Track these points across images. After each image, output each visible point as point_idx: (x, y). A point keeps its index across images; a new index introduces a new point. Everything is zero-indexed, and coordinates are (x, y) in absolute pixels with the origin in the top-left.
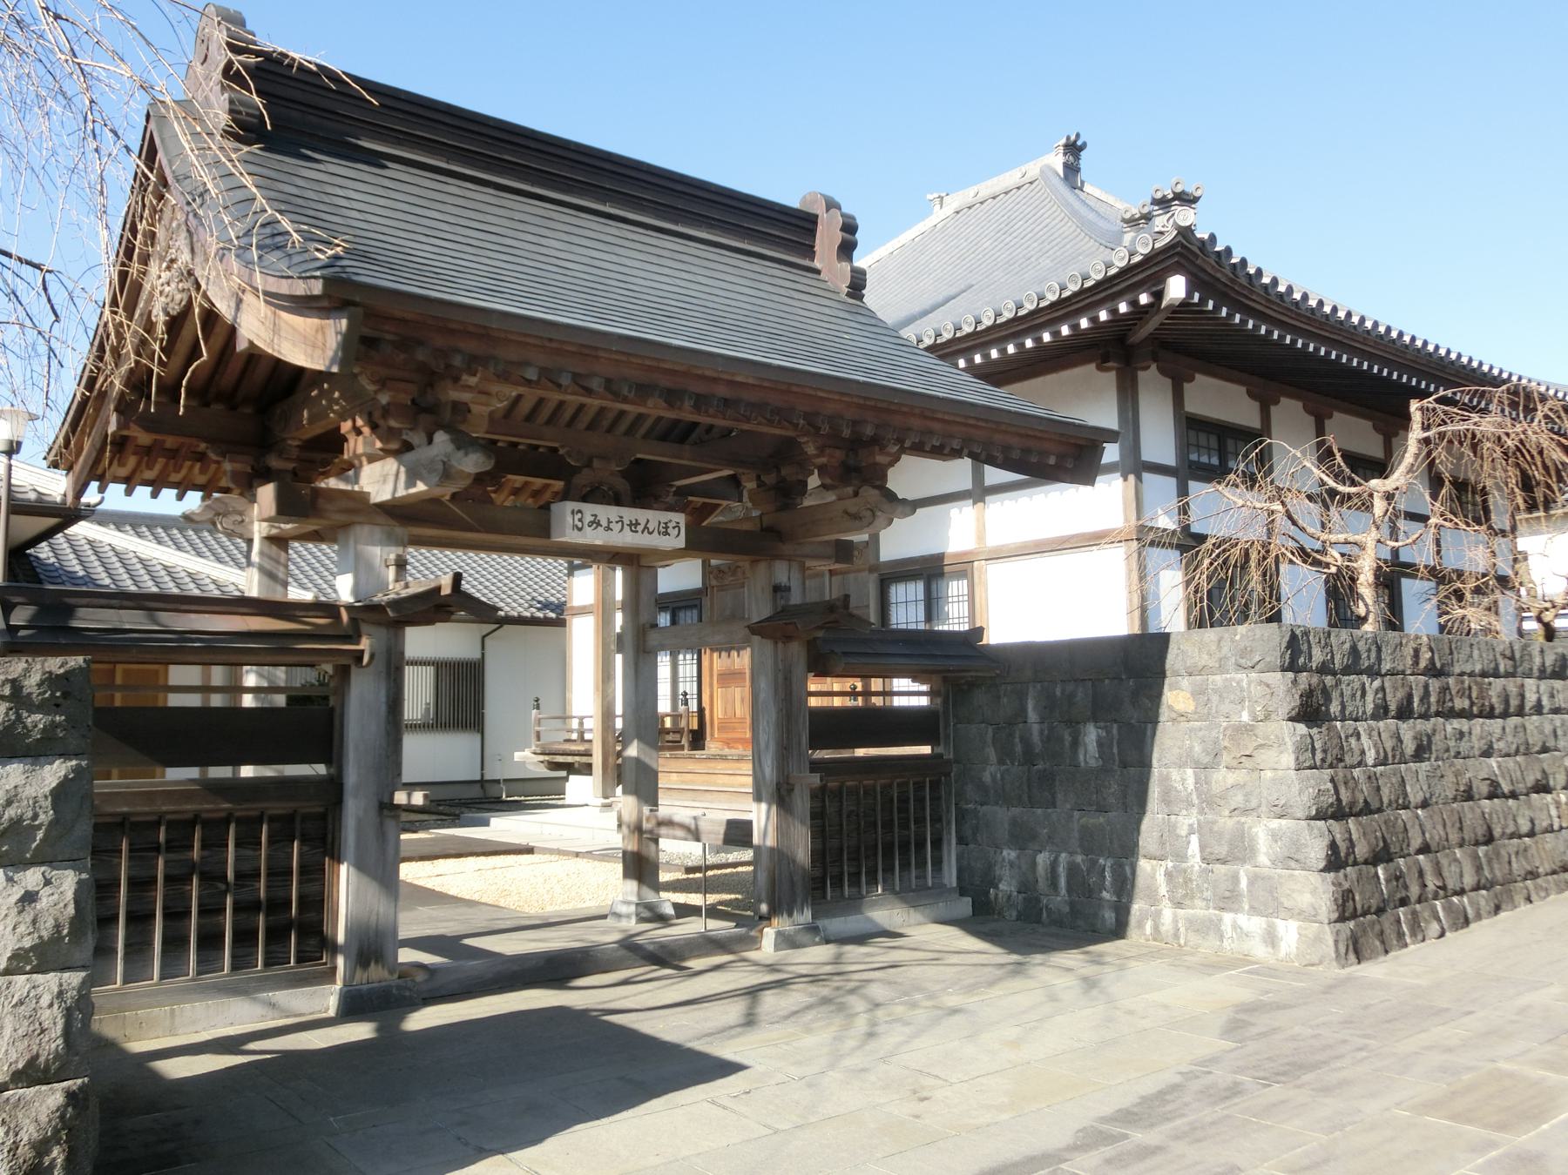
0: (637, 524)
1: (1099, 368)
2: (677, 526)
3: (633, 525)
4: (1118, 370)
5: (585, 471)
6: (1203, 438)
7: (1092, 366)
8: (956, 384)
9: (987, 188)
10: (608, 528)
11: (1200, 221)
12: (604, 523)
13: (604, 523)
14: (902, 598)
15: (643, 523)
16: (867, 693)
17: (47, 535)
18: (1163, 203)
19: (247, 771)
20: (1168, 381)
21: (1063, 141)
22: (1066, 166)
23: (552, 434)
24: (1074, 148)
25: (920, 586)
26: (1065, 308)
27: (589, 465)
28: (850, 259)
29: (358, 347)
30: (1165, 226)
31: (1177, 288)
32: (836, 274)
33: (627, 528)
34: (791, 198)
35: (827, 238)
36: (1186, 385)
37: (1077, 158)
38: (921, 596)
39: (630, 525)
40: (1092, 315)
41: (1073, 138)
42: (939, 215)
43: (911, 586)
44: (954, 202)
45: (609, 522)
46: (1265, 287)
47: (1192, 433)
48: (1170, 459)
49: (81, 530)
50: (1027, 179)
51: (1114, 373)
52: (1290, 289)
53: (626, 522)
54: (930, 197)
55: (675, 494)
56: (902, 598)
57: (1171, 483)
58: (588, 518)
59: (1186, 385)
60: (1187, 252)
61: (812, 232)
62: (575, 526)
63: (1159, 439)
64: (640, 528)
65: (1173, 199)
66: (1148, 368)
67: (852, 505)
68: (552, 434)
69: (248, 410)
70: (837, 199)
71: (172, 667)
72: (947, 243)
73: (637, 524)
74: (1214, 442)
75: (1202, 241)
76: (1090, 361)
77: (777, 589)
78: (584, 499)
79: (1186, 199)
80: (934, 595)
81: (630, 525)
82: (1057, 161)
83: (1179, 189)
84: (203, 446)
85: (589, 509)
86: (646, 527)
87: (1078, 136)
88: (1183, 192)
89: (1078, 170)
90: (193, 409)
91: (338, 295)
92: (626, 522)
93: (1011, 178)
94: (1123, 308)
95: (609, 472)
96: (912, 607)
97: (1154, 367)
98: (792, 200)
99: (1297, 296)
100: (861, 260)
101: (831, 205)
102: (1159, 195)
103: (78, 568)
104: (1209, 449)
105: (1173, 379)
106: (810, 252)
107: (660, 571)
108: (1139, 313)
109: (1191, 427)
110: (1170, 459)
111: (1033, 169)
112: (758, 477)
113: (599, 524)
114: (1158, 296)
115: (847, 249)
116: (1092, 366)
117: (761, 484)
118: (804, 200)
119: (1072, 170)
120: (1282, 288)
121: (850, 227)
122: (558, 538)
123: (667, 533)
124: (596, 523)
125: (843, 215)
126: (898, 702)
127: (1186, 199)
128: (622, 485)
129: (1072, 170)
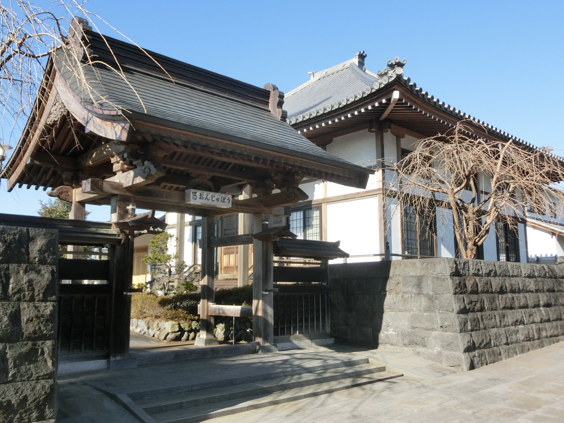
4: (376, 132)
7: (367, 130)
9: (330, 70)
11: (405, 73)
14: (295, 218)
18: (392, 66)
20: (395, 137)
21: (358, 53)
22: (359, 62)
23: (173, 162)
24: (362, 57)
25: (302, 212)
28: (282, 108)
30: (392, 75)
31: (396, 95)
32: (277, 114)
34: (261, 85)
35: (273, 100)
37: (363, 60)
38: (302, 217)
40: (366, 107)
41: (362, 53)
42: (313, 79)
43: (298, 213)
44: (318, 75)
46: (417, 91)
51: (374, 133)
52: (444, 104)
54: (309, 73)
56: (295, 218)
60: (399, 83)
61: (268, 97)
65: (395, 65)
68: (173, 162)
70: (277, 86)
72: (313, 83)
75: (405, 81)
76: (365, 128)
79: (400, 65)
80: (307, 216)
82: (356, 61)
83: (397, 61)
86: (206, 198)
87: (364, 52)
88: (399, 62)
89: (363, 64)
90: (61, 155)
93: (340, 67)
94: (377, 104)
98: (261, 86)
99: (446, 106)
100: (285, 107)
101: (275, 88)
102: (390, 63)
105: (397, 137)
106: (267, 103)
108: (384, 107)
111: (348, 63)
114: (389, 100)
115: (280, 104)
116: (367, 130)
118: (265, 86)
119: (361, 64)
120: (441, 103)
121: (281, 96)
123: (224, 202)
125: (279, 92)
126: (292, 265)
127: (400, 65)
129: (361, 64)
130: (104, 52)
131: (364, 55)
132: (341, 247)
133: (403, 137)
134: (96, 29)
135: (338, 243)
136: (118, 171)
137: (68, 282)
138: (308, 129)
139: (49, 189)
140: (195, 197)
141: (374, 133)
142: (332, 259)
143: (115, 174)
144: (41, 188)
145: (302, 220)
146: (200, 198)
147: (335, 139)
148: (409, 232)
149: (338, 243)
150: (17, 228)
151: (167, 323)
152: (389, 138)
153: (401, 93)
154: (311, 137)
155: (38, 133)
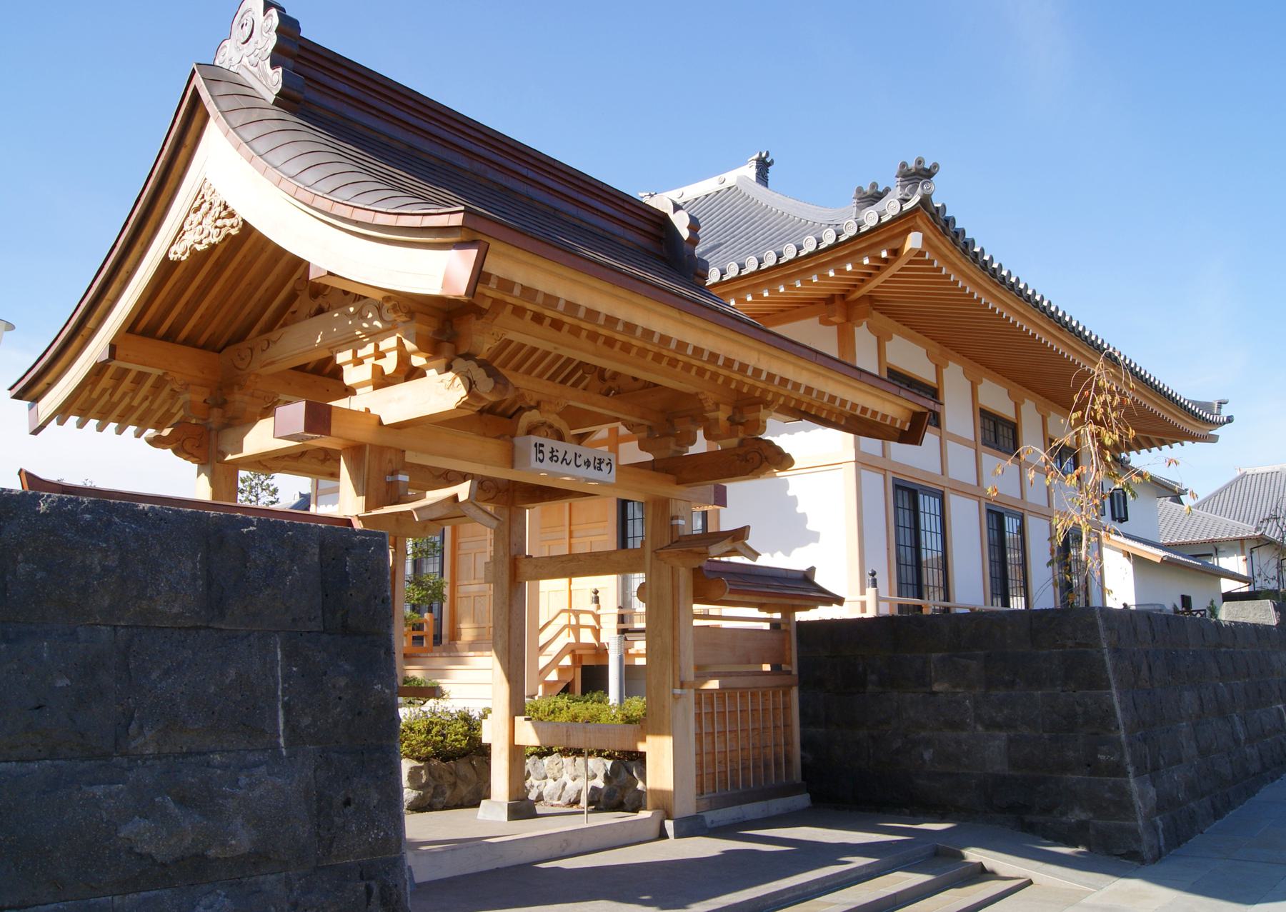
7: (817, 319)
11: (941, 192)
21: (757, 156)
24: (763, 167)
31: (914, 241)
50: (727, 184)
51: (835, 328)
82: (750, 171)
86: (564, 459)
87: (767, 154)
114: (895, 253)
116: (817, 319)
131: (768, 160)
132: (819, 579)
135: (812, 570)
137: (714, 684)
139: (150, 432)
140: (540, 456)
141: (835, 328)
142: (806, 608)
144: (131, 429)
146: (551, 459)
149: (812, 570)
153: (925, 239)
155: (951, 256)
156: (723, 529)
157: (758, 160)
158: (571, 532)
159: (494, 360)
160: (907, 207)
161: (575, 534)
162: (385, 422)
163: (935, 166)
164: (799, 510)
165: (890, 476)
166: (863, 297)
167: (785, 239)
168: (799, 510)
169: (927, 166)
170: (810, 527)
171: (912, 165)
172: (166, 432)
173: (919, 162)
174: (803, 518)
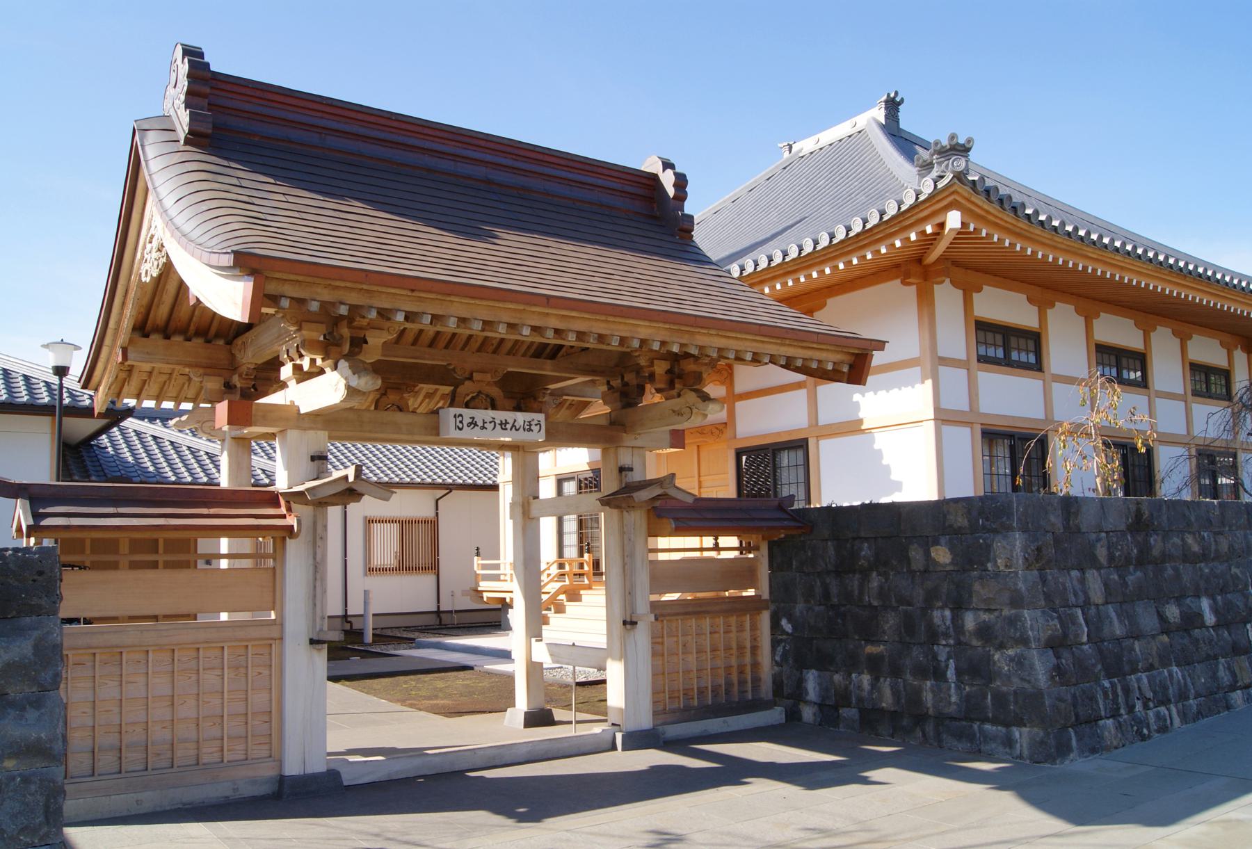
0: (507, 423)
1: (904, 283)
2: (539, 424)
3: (503, 425)
5: (467, 383)
6: (990, 336)
7: (898, 281)
8: (763, 308)
10: (484, 428)
12: (480, 424)
13: (480, 424)
15: (511, 421)
16: (716, 548)
17: (105, 430)
19: (224, 616)
21: (885, 98)
26: (868, 237)
27: (470, 378)
29: (260, 298)
33: (498, 427)
36: (975, 295)
39: (501, 424)
45: (484, 422)
47: (981, 334)
48: (961, 354)
49: (130, 423)
50: (858, 128)
51: (914, 287)
53: (498, 422)
55: (551, 394)
57: (963, 373)
58: (466, 421)
59: (975, 295)
62: (457, 427)
63: (955, 339)
64: (509, 426)
66: (942, 282)
67: (676, 403)
69: (221, 342)
70: (672, 161)
71: (329, 508)
73: (507, 423)
74: (999, 338)
76: (897, 277)
77: (622, 470)
78: (467, 406)
81: (501, 424)
84: (187, 370)
85: (468, 413)
86: (513, 425)
87: (896, 93)
91: (245, 263)
92: (498, 422)
95: (486, 383)
96: (793, 471)
97: (948, 280)
101: (667, 165)
103: (130, 459)
104: (995, 345)
107: (541, 455)
109: (984, 329)
110: (961, 354)
112: (608, 383)
113: (476, 425)
114: (942, 225)
116: (898, 281)
117: (610, 388)
122: (443, 436)
123: (530, 430)
124: (473, 424)
128: (495, 392)
130: (238, 124)
131: (898, 99)
133: (979, 290)
134: (219, 63)
136: (289, 379)
138: (784, 284)
141: (914, 287)
143: (283, 385)
145: (1008, 460)
147: (830, 301)
148: (995, 477)
150: (1114, 481)
151: (30, 648)
152: (947, 296)
154: (789, 300)
156: (649, 477)
157: (886, 102)
158: (700, 482)
159: (120, 430)
160: (940, 185)
161: (704, 484)
162: (302, 411)
163: (969, 141)
164: (884, 462)
165: (978, 429)
166: (938, 260)
167: (882, 197)
168: (884, 462)
169: (962, 141)
170: (894, 477)
171: (945, 142)
172: (735, 271)
173: (953, 137)
174: (887, 469)
